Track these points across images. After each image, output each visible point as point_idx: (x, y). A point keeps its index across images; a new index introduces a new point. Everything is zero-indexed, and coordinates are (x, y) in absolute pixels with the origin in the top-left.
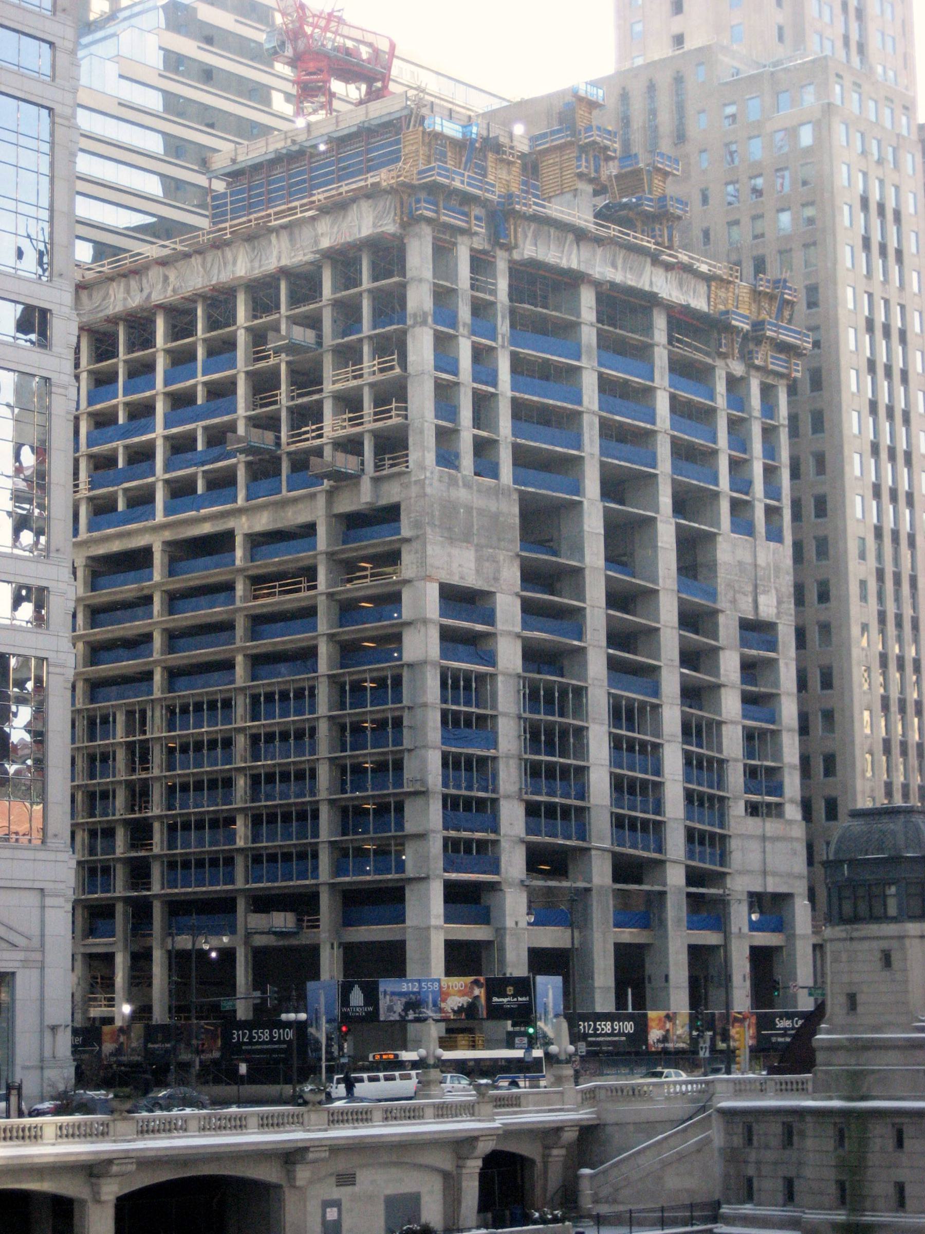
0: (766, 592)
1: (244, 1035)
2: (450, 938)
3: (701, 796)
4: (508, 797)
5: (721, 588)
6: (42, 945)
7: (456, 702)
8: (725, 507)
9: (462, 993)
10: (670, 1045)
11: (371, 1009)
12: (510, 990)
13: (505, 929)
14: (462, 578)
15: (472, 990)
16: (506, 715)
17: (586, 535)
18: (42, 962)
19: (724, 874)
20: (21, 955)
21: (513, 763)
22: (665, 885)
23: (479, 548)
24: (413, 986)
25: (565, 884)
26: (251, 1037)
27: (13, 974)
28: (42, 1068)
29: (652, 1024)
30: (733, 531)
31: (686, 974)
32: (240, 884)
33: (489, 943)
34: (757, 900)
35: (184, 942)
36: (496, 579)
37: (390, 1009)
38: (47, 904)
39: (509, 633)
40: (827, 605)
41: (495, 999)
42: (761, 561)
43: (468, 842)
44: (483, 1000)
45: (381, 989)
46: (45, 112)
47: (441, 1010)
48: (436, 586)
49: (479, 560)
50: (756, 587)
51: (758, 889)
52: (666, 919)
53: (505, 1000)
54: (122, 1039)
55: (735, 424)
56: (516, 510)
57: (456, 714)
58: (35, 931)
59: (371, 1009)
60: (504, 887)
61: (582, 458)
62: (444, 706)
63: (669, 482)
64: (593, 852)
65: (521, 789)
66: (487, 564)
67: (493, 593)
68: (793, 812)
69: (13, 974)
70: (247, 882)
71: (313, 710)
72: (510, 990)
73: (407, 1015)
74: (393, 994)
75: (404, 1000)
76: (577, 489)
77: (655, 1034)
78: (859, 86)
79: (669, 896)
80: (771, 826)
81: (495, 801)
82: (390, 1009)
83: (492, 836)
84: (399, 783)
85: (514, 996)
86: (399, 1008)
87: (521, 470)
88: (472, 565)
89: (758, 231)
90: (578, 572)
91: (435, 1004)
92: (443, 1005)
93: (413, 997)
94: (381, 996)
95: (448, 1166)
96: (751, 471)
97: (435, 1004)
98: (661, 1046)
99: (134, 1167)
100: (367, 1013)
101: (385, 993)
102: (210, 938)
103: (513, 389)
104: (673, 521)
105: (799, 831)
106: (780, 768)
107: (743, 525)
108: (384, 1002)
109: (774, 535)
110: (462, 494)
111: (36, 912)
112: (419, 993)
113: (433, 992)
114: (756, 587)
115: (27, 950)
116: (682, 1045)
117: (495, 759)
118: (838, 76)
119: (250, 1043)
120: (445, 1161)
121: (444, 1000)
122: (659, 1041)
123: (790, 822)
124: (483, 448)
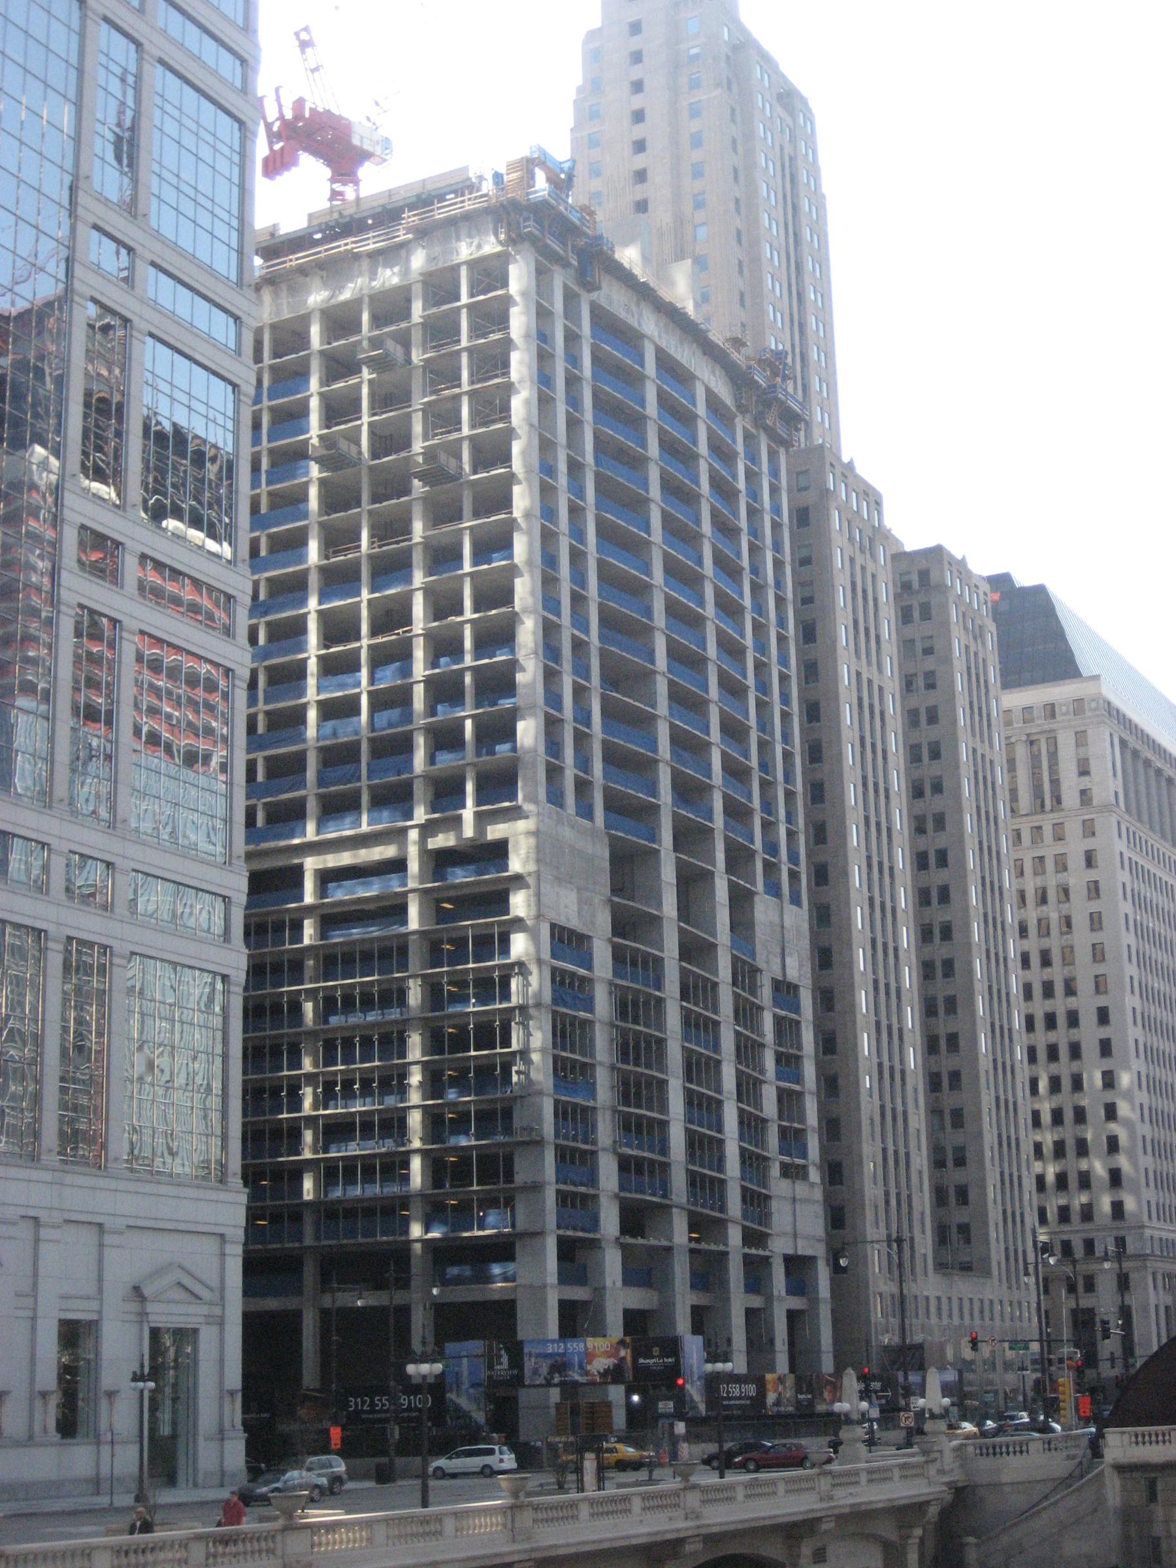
0: (791, 955)
1: (363, 1403)
2: (566, 1297)
3: (639, 1162)
4: (604, 1149)
5: (758, 947)
6: (222, 1298)
7: (564, 1049)
8: (759, 866)
9: (608, 1355)
10: (782, 1409)
11: (516, 1372)
12: (656, 1351)
13: (604, 1288)
14: (568, 920)
15: (618, 1351)
16: (601, 1064)
17: (663, 885)
18: (222, 1317)
19: (767, 1235)
20: (204, 1310)
21: (608, 1114)
22: (726, 1245)
23: (579, 889)
24: (559, 1347)
25: (640, 1241)
26: (372, 1405)
27: (195, 1331)
28: (222, 1440)
29: (769, 1386)
30: (766, 893)
31: (744, 1338)
32: (308, 1241)
33: (585, 1303)
34: (789, 1260)
35: (327, 1301)
36: (593, 923)
37: (535, 1372)
38: (227, 1251)
39: (602, 979)
40: (830, 971)
41: (641, 1361)
42: (787, 924)
43: (575, 1195)
44: (629, 1359)
45: (526, 1350)
46: (230, 388)
47: (587, 1373)
48: (548, 926)
49: (580, 902)
50: (783, 949)
51: (791, 1252)
52: (728, 1282)
53: (651, 1361)
54: (780, 1388)
55: (765, 785)
56: (607, 855)
57: (564, 1059)
58: (215, 1282)
59: (516, 1372)
60: (603, 1244)
61: (659, 806)
62: (556, 1052)
63: (722, 836)
64: (674, 1210)
65: (615, 1142)
66: (586, 907)
67: (589, 938)
68: (814, 1175)
69: (195, 1331)
70: (317, 1238)
71: (403, 1055)
72: (656, 1351)
73: (552, 1378)
74: (539, 1355)
75: (549, 1362)
76: (654, 836)
77: (771, 1397)
78: (846, 477)
79: (731, 1256)
80: (801, 1189)
81: (594, 1153)
82: (535, 1372)
83: (592, 1191)
84: (508, 1130)
85: (661, 1356)
86: (544, 1370)
87: (613, 816)
88: (575, 908)
89: (807, 594)
90: (656, 921)
91: (581, 1367)
92: (589, 1367)
93: (559, 1359)
94: (526, 1359)
95: (893, 1536)
96: (778, 833)
97: (581, 1367)
98: (776, 1409)
99: (701, 1545)
100: (512, 1376)
101: (530, 1355)
102: (365, 1293)
103: (604, 732)
104: (726, 876)
105: (818, 1194)
106: (804, 1130)
107: (773, 889)
108: (529, 1364)
109: (796, 900)
110: (567, 833)
111: (216, 1260)
112: (564, 1354)
113: (579, 1353)
114: (783, 949)
115: (210, 1304)
116: (791, 1409)
117: (594, 1109)
118: (831, 465)
119: (372, 1411)
120: (889, 1531)
121: (589, 1363)
122: (774, 1404)
123: (812, 1185)
124: (583, 787)
